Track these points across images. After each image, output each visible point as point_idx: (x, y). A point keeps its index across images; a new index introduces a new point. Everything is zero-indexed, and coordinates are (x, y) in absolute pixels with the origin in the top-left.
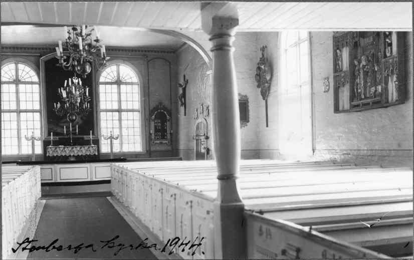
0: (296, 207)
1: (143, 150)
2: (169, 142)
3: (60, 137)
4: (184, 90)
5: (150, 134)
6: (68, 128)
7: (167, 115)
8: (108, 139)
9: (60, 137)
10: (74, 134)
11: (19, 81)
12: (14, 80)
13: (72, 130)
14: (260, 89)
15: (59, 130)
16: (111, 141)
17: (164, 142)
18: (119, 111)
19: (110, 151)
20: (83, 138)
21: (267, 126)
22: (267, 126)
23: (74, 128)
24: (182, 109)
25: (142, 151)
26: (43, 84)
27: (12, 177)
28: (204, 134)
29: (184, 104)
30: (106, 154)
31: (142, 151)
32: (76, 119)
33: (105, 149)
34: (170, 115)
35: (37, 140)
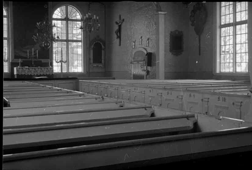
0: (24, 130)
1: (84, 71)
2: (103, 66)
3: (24, 60)
4: (120, 26)
5: (90, 59)
6: (30, 53)
7: (102, 45)
8: (59, 62)
9: (24, 60)
10: (36, 58)
11: (68, 21)
12: (65, 18)
13: (34, 55)
14: (194, 27)
15: (23, 55)
16: (62, 64)
17: (100, 65)
18: (67, 41)
19: (60, 72)
20: (41, 61)
21: (200, 54)
22: (200, 54)
23: (35, 53)
24: (116, 41)
25: (9, 72)
26: (214, 22)
27: (129, 89)
28: (144, 60)
29: (119, 37)
30: (57, 74)
31: (9, 72)
32: (50, 45)
33: (56, 69)
34: (105, 46)
35: (64, 62)
